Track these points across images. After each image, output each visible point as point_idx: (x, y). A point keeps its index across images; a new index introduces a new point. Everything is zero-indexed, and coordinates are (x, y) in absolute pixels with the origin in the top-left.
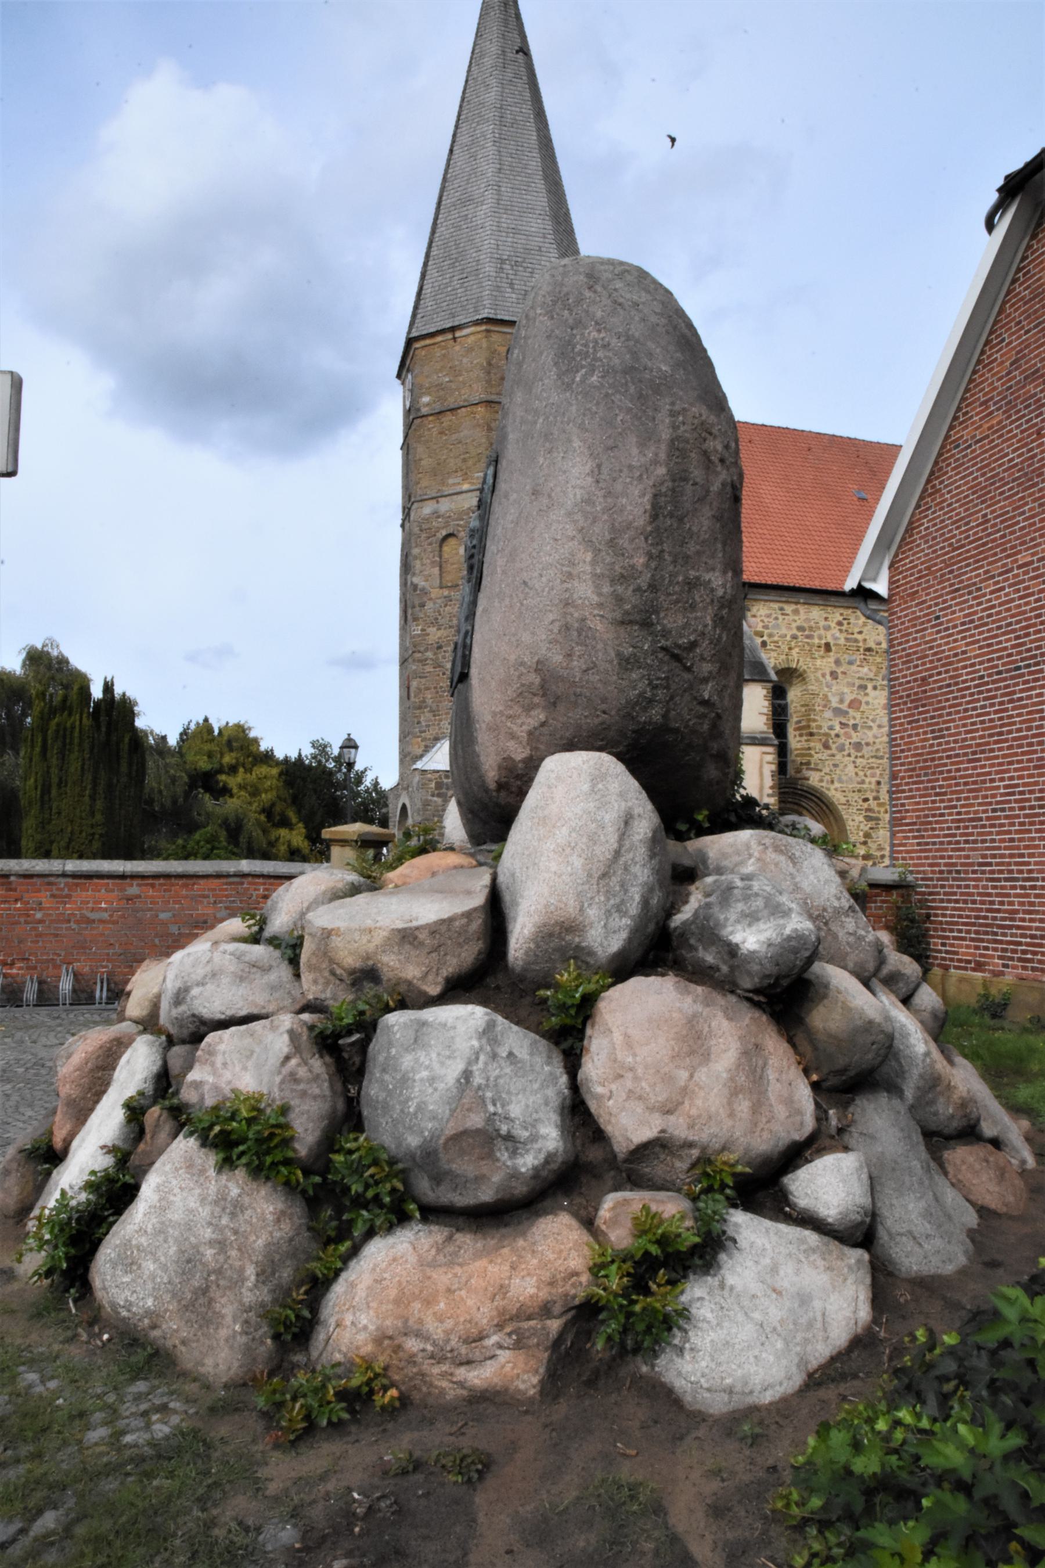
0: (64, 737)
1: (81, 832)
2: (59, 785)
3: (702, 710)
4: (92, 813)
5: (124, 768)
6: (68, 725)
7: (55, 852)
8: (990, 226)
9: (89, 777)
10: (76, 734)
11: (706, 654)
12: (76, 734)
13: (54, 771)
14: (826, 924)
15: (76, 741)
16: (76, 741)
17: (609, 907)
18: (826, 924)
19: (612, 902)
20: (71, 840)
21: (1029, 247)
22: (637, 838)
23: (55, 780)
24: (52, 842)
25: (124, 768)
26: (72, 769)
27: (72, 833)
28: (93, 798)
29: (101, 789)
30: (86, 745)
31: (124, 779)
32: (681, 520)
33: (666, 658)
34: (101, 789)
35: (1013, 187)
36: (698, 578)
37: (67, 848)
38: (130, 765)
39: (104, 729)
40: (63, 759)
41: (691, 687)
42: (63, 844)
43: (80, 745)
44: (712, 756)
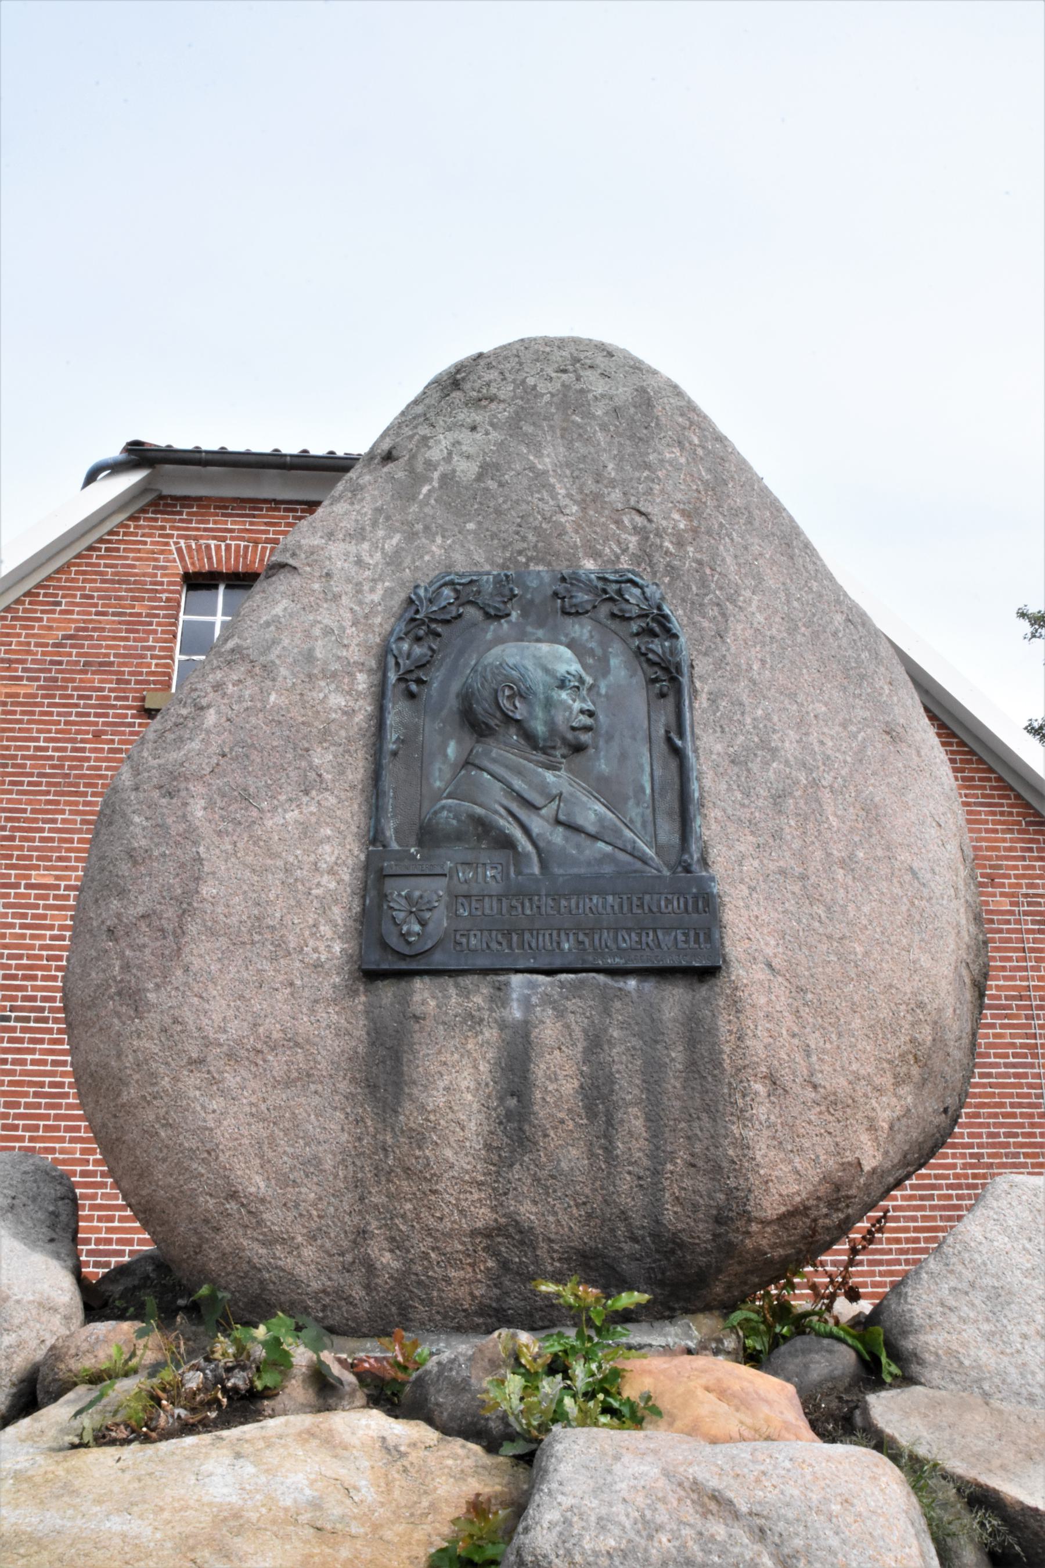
8: (91, 477)
21: (122, 525)
35: (139, 455)
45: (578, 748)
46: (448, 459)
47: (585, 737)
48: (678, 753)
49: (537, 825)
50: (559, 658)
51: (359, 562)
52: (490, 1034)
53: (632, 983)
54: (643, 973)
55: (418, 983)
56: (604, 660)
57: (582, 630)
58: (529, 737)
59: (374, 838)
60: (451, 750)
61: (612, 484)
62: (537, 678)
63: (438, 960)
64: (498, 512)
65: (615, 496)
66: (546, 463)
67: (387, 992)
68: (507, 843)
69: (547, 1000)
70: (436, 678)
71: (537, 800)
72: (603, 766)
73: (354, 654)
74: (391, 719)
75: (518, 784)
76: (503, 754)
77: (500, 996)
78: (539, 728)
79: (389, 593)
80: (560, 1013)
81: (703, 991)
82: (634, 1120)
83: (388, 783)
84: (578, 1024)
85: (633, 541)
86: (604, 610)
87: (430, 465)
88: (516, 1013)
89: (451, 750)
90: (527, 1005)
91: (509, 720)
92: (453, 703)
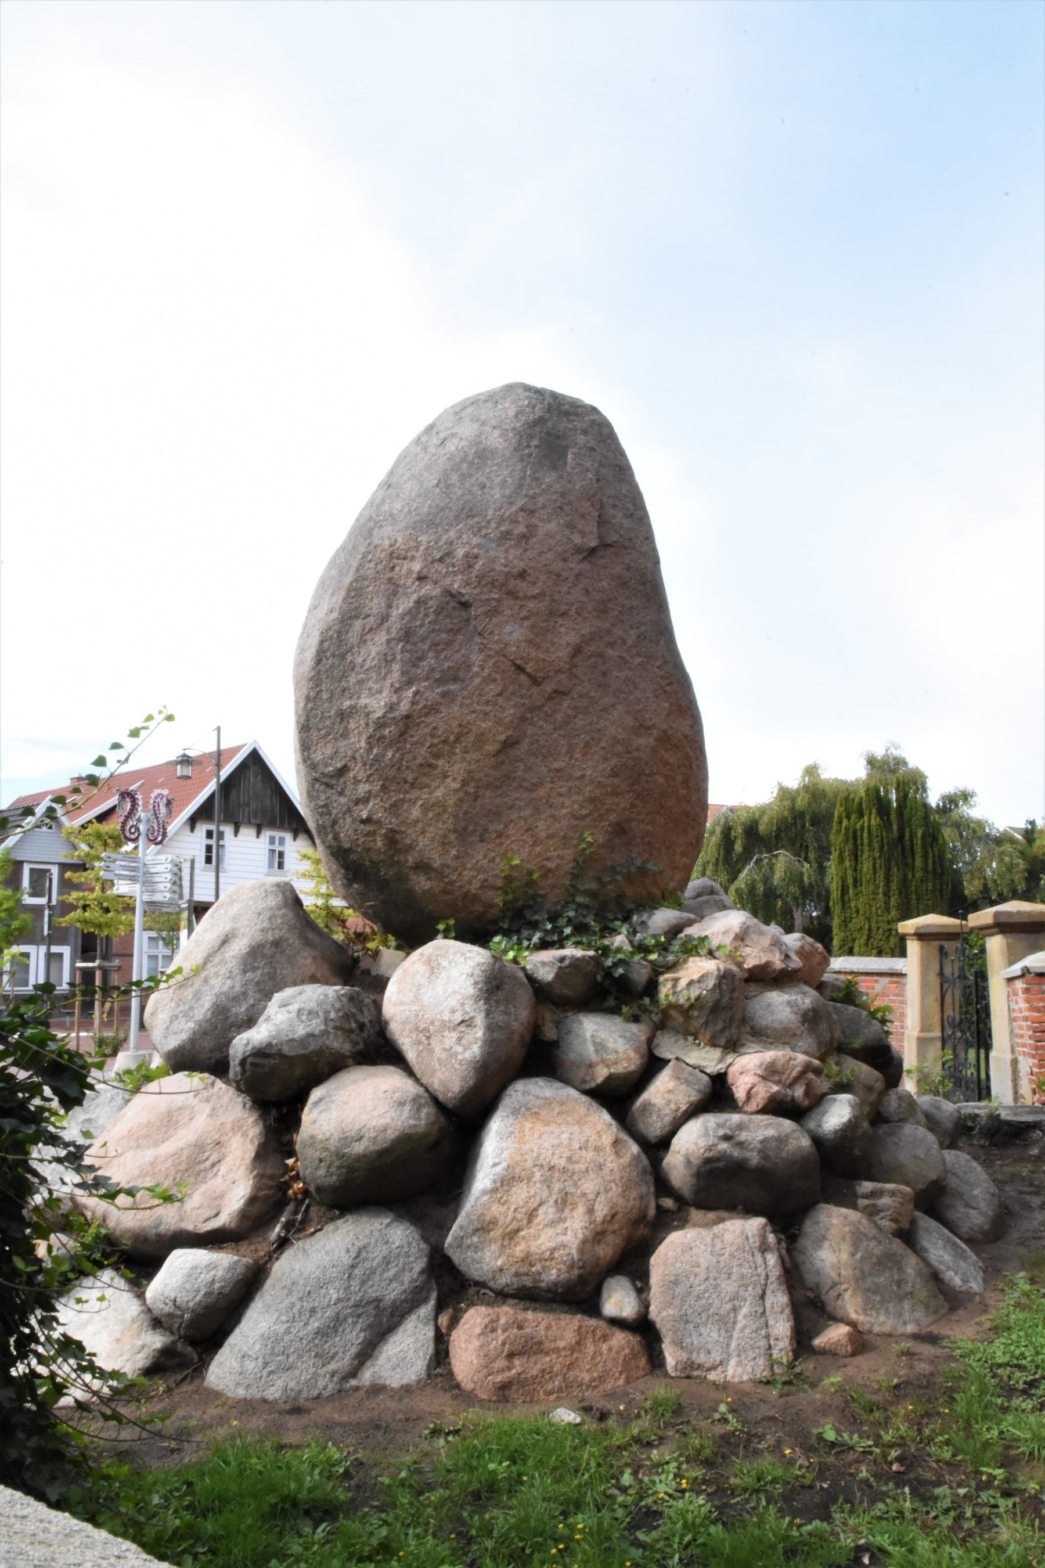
0: (855, 838)
1: (878, 928)
2: (855, 886)
3: (368, 828)
4: (887, 909)
5: (919, 862)
6: (858, 827)
7: (856, 950)
9: (881, 874)
10: (865, 835)
11: (362, 776)
12: (865, 835)
13: (849, 872)
14: (428, 1038)
15: (866, 841)
16: (866, 841)
17: (177, 1012)
18: (428, 1038)
19: (181, 1008)
20: (869, 937)
22: (231, 953)
23: (850, 881)
24: (854, 940)
25: (919, 862)
26: (865, 869)
27: (870, 929)
28: (887, 895)
29: (894, 886)
30: (876, 845)
31: (919, 874)
32: (343, 657)
33: (322, 788)
34: (894, 886)
36: (351, 707)
37: (867, 945)
38: (925, 857)
39: (895, 827)
40: (856, 860)
41: (349, 810)
42: (863, 941)
43: (870, 844)
44: (411, 868)
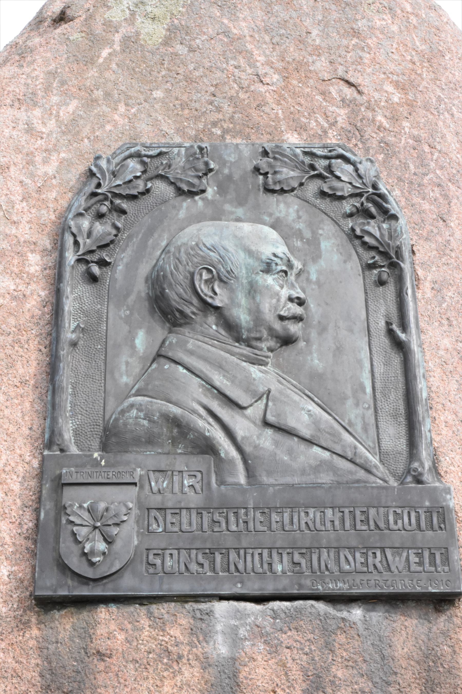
45: (287, 341)
46: (131, 21)
47: (294, 328)
48: (400, 346)
49: (242, 426)
50: (264, 239)
51: (30, 130)
52: (191, 673)
53: (357, 613)
54: (369, 600)
55: (103, 613)
56: (314, 243)
57: (287, 208)
58: (231, 327)
59: (50, 440)
60: (141, 340)
61: (317, 51)
62: (239, 261)
63: (128, 584)
64: (189, 80)
65: (321, 65)
66: (242, 27)
67: (65, 624)
68: (208, 448)
69: (259, 633)
70: (122, 259)
71: (243, 400)
72: (316, 361)
73: (25, 232)
74: (69, 305)
75: (218, 380)
76: (201, 344)
77: (201, 630)
78: (242, 317)
79: (65, 165)
80: (274, 649)
81: (441, 622)
82: (356, 485)
83: (66, 377)
84: (295, 661)
85: (342, 114)
86: (313, 187)
87: (110, 26)
88: (221, 648)
89: (141, 340)
90: (235, 639)
91: (207, 307)
92: (141, 287)
